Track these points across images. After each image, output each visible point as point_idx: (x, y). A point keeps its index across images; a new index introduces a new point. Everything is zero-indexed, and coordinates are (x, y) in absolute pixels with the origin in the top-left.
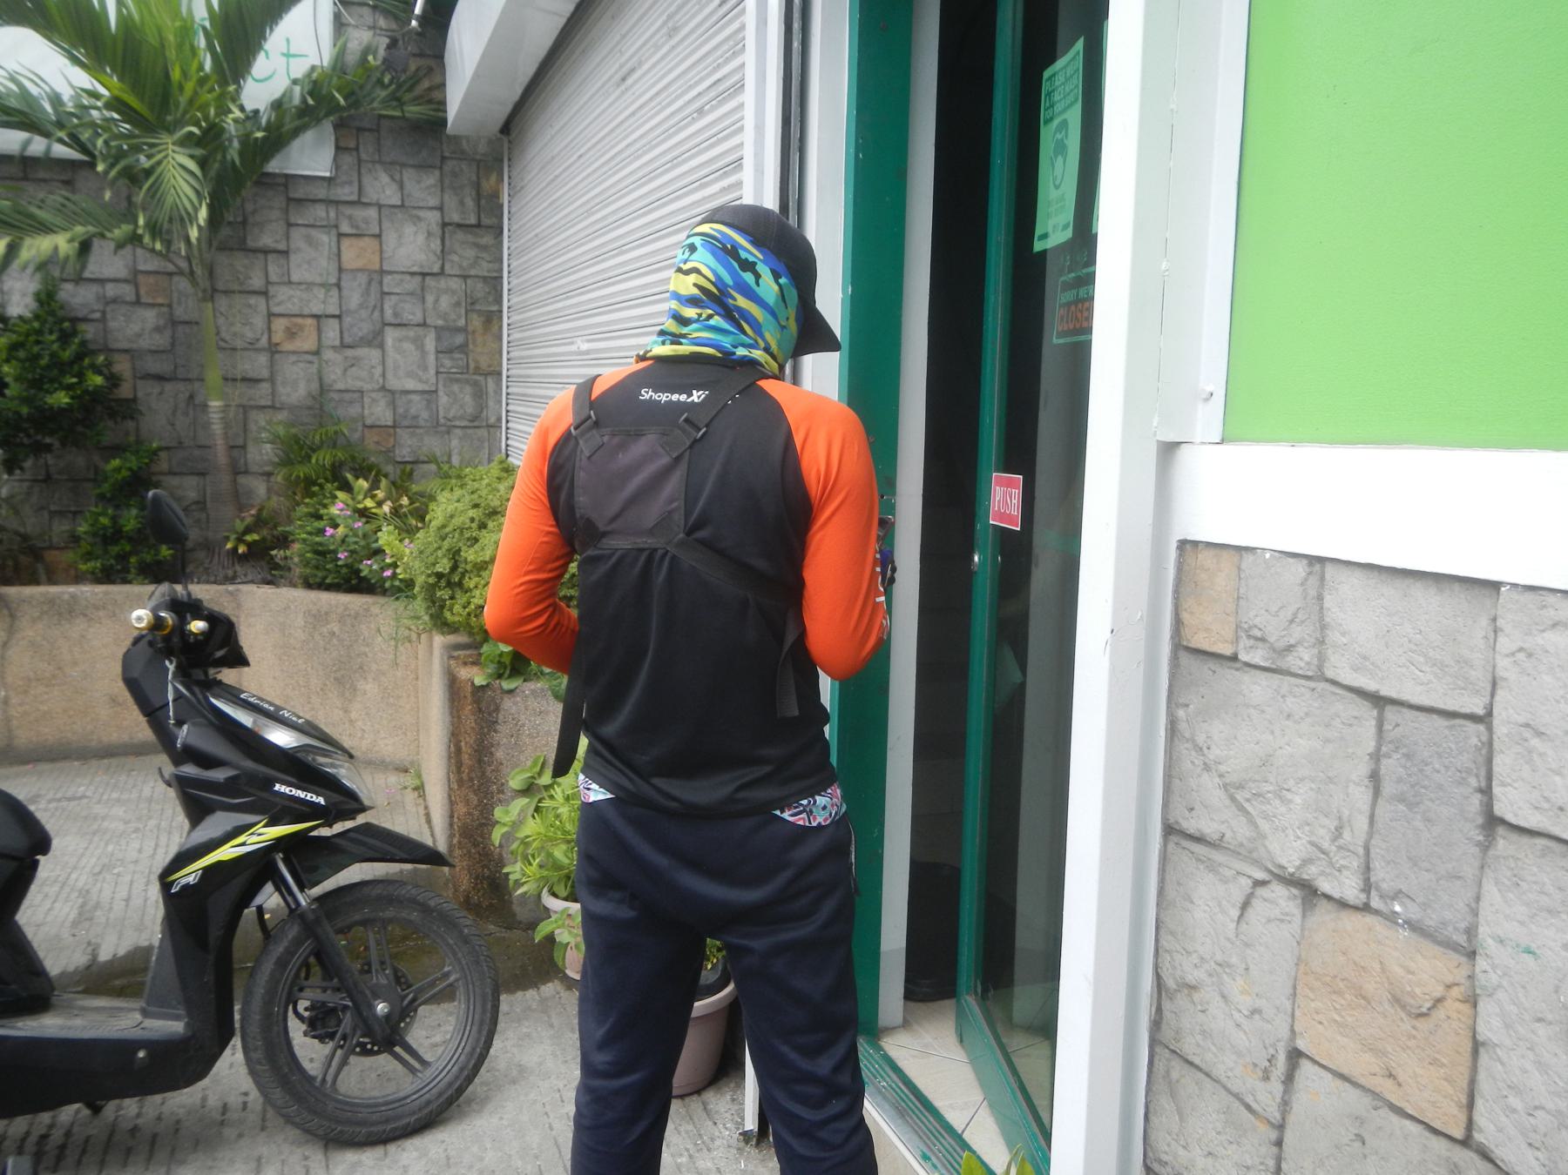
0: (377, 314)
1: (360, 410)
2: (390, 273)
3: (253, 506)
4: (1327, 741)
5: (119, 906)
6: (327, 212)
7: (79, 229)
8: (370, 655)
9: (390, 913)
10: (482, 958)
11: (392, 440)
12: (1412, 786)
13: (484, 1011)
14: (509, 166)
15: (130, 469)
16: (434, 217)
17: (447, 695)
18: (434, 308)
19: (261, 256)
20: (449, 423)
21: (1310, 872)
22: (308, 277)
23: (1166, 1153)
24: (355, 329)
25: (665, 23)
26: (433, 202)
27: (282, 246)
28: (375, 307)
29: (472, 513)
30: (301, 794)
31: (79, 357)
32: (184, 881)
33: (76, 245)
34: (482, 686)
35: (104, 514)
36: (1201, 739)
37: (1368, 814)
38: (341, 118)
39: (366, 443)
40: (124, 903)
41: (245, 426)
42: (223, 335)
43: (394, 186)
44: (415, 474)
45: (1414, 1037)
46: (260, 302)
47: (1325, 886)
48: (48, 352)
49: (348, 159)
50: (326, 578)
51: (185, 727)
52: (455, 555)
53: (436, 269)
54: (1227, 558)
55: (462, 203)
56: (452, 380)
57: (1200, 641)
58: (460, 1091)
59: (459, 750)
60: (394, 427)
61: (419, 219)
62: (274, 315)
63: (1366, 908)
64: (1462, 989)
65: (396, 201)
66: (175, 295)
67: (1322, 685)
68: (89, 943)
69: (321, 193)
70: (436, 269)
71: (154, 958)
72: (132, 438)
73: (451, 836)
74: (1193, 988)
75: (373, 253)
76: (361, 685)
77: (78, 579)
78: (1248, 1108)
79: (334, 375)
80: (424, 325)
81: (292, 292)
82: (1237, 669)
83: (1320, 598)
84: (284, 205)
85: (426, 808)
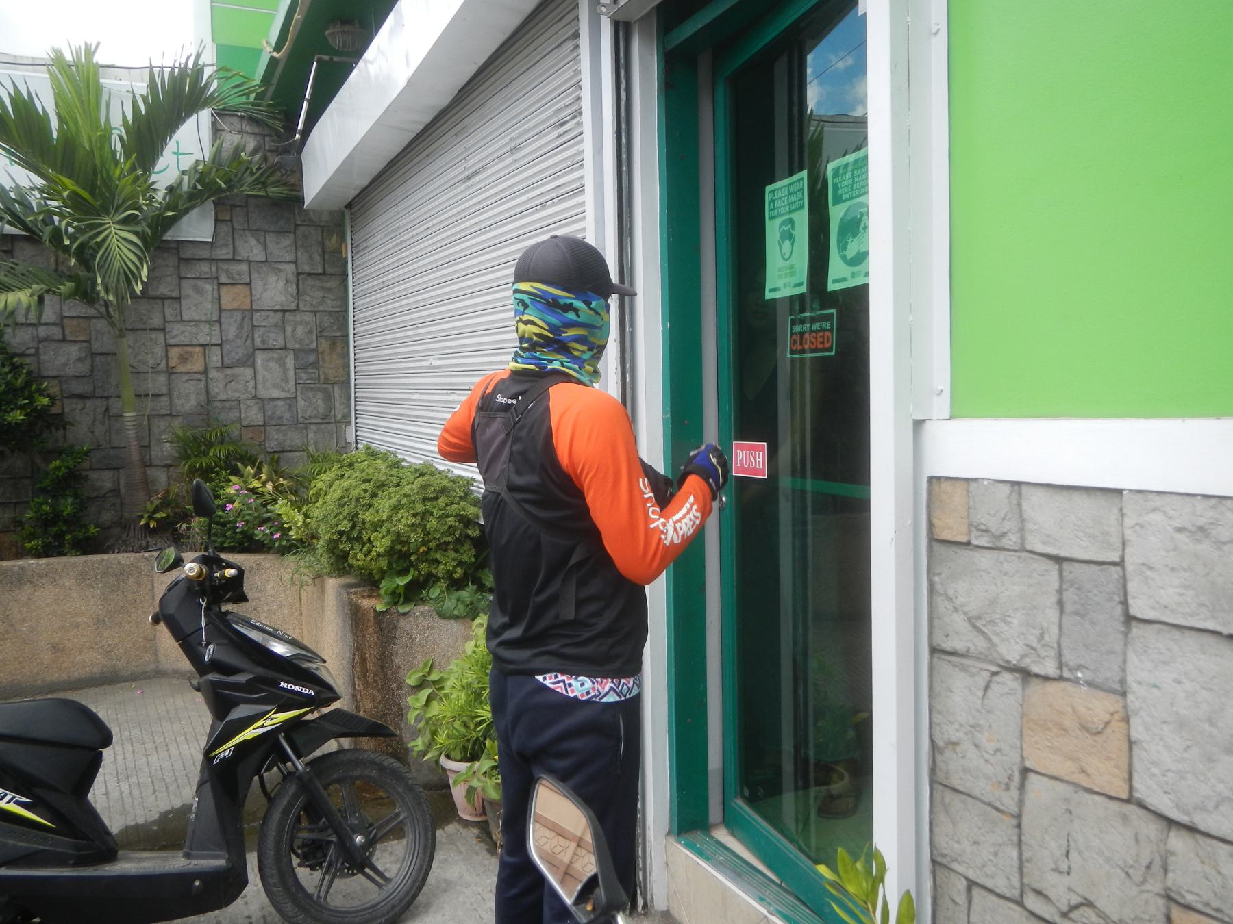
0: (249, 342)
1: (238, 415)
3: (157, 492)
4: (1031, 585)
6: (211, 268)
9: (357, 772)
11: (263, 435)
15: (67, 467)
16: (290, 269)
18: (293, 336)
19: (160, 302)
20: (306, 421)
21: (1026, 662)
22: (197, 317)
23: (946, 849)
24: (233, 354)
26: (290, 257)
27: (175, 294)
28: (247, 337)
29: (364, 486)
30: (298, 689)
31: (28, 384)
32: (222, 756)
33: (36, 298)
34: (383, 612)
35: (46, 503)
36: (951, 593)
37: (1057, 624)
38: (219, 199)
40: (105, 797)
43: (260, 248)
45: (1096, 747)
46: (160, 336)
47: (1036, 669)
49: (225, 228)
50: (224, 542)
51: (211, 647)
52: (353, 517)
53: (293, 307)
54: (960, 488)
55: (311, 257)
56: (307, 389)
57: (946, 535)
58: (415, 896)
59: (364, 661)
60: (264, 426)
61: (280, 270)
63: (1061, 678)
64: (1120, 714)
65: (261, 257)
66: (93, 333)
67: (1024, 555)
69: (205, 253)
70: (293, 307)
74: (955, 744)
75: (245, 297)
77: (18, 556)
78: (997, 809)
79: (217, 388)
80: (285, 348)
81: (184, 328)
82: (970, 550)
83: (1019, 505)
84: (176, 263)
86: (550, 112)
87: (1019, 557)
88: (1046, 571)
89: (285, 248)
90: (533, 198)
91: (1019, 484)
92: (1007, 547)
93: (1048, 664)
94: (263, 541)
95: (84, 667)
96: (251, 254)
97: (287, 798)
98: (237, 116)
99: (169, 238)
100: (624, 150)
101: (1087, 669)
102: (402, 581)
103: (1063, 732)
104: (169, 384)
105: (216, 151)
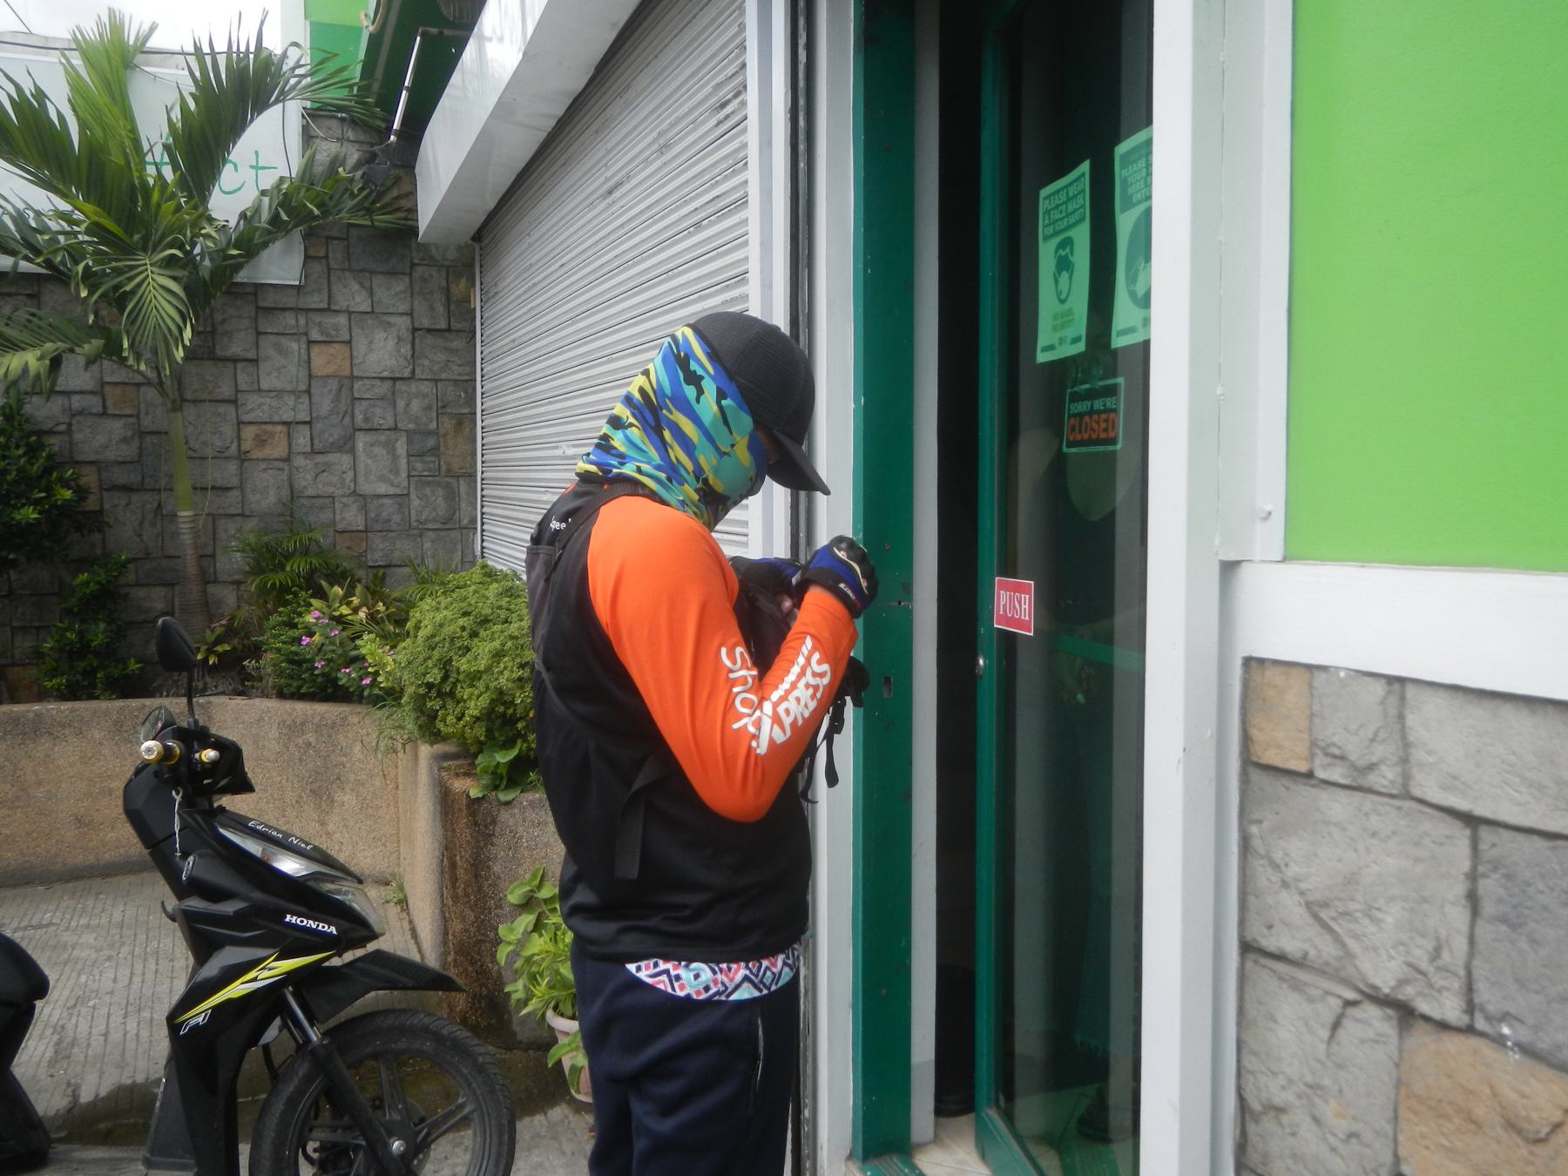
0: (347, 420)
2: (361, 378)
3: (223, 616)
4: (1418, 860)
5: (97, 1041)
6: (297, 321)
7: (49, 346)
8: (348, 765)
10: (497, 1087)
11: (364, 544)
12: (1515, 907)
13: (500, 1144)
14: (481, 272)
16: (403, 323)
17: (439, 808)
19: (230, 365)
20: (421, 526)
21: (1407, 994)
22: (279, 385)
24: (326, 435)
25: (655, 140)
26: (403, 308)
27: (251, 355)
29: (461, 622)
30: (312, 924)
31: (47, 471)
32: (193, 1022)
33: (47, 362)
35: (70, 629)
36: (1278, 856)
38: (311, 228)
39: (338, 548)
41: (214, 533)
42: (192, 444)
43: (365, 294)
44: (388, 578)
47: (1424, 1007)
48: (15, 467)
49: (318, 268)
50: (301, 687)
51: (191, 859)
52: (446, 665)
53: (407, 373)
55: (431, 308)
57: (1271, 757)
59: (453, 866)
60: (366, 531)
62: (244, 423)
63: (1470, 1030)
65: (366, 307)
66: (142, 405)
67: (1408, 804)
68: (69, 1084)
69: (291, 301)
70: (407, 373)
71: (158, 1104)
72: (98, 551)
73: (445, 954)
74: (1280, 1110)
75: (344, 359)
76: (339, 797)
77: (42, 696)
79: (305, 481)
80: (395, 429)
81: (262, 400)
82: (1313, 786)
83: (1401, 717)
84: (253, 314)
85: (411, 922)
86: (708, 89)
87: (1399, 808)
88: (1447, 837)
89: (397, 294)
90: (686, 215)
91: (1402, 680)
92: (1377, 787)
93: (1448, 1002)
94: (348, 688)
95: (117, 847)
96: (352, 303)
97: (296, 1082)
98: (336, 117)
99: (246, 281)
100: (802, 137)
101: (1522, 1022)
102: (503, 758)
103: (1473, 1127)
104: (241, 474)
105: (307, 164)
